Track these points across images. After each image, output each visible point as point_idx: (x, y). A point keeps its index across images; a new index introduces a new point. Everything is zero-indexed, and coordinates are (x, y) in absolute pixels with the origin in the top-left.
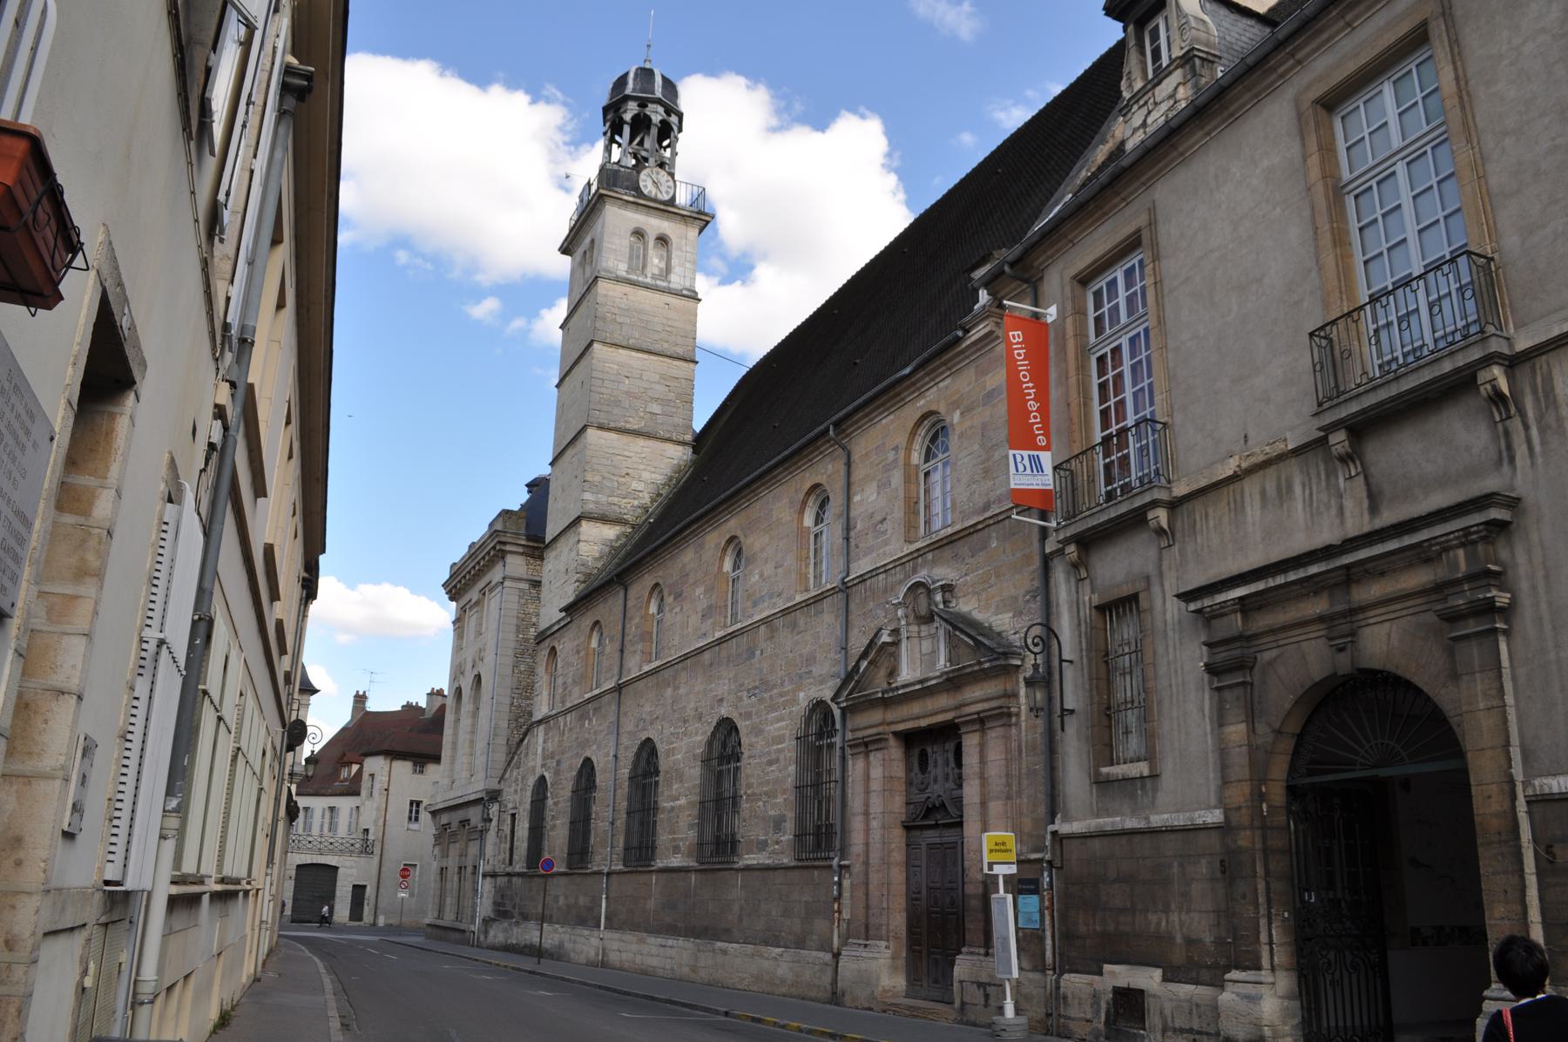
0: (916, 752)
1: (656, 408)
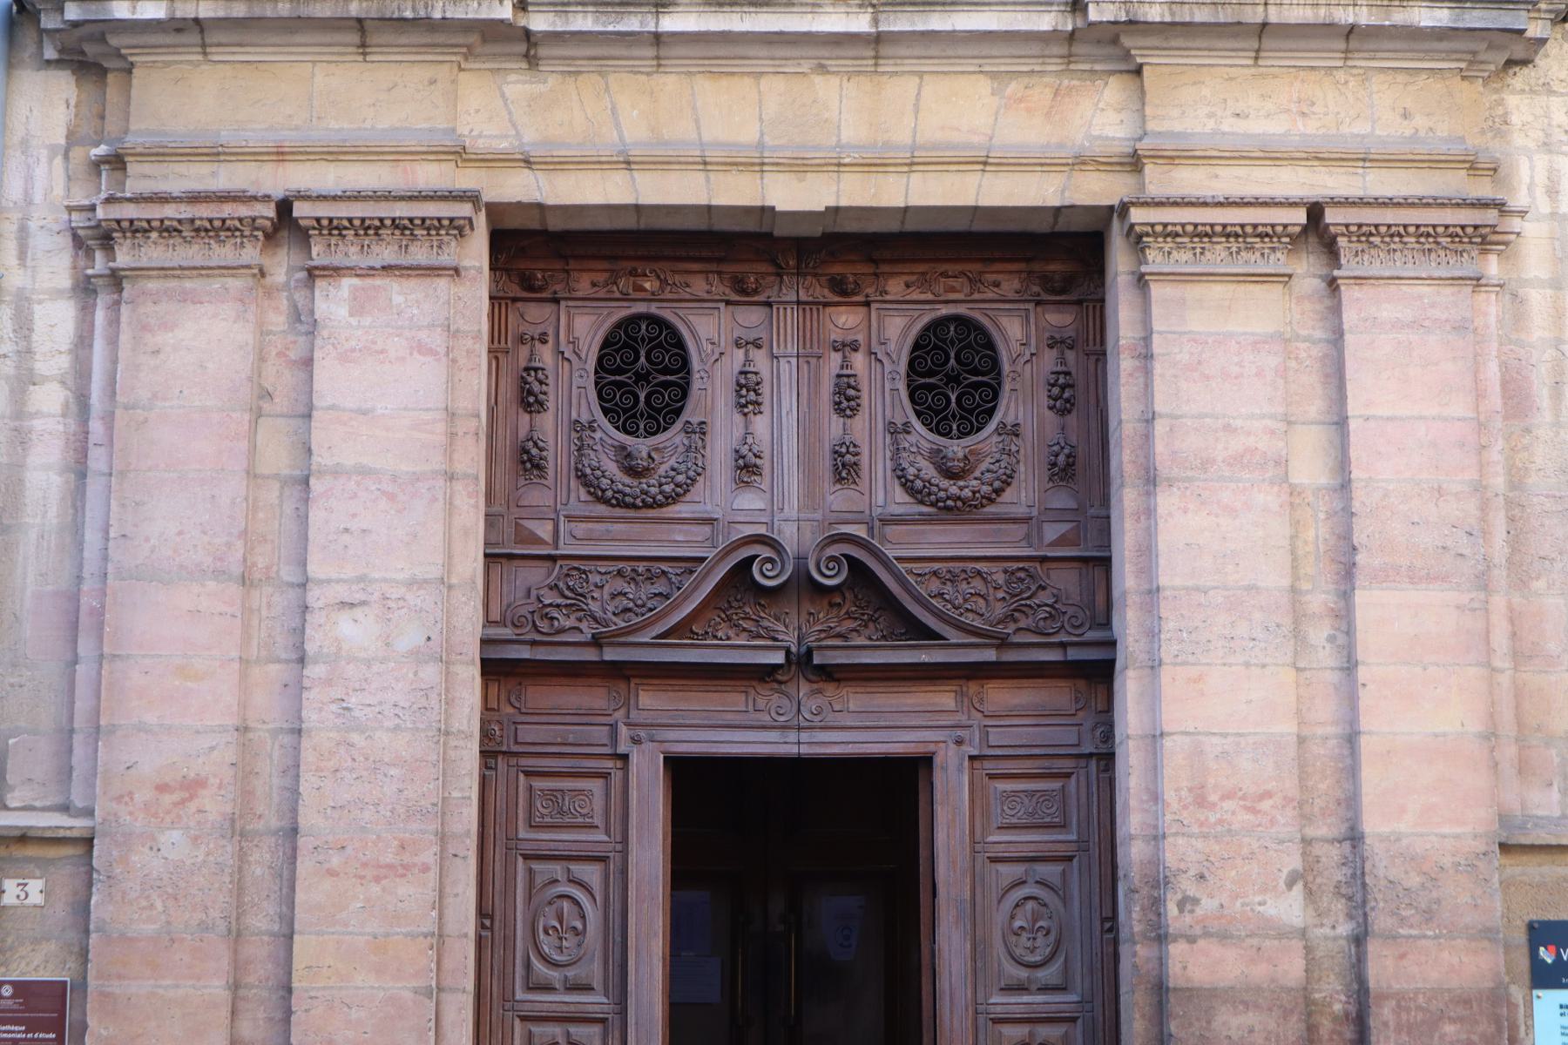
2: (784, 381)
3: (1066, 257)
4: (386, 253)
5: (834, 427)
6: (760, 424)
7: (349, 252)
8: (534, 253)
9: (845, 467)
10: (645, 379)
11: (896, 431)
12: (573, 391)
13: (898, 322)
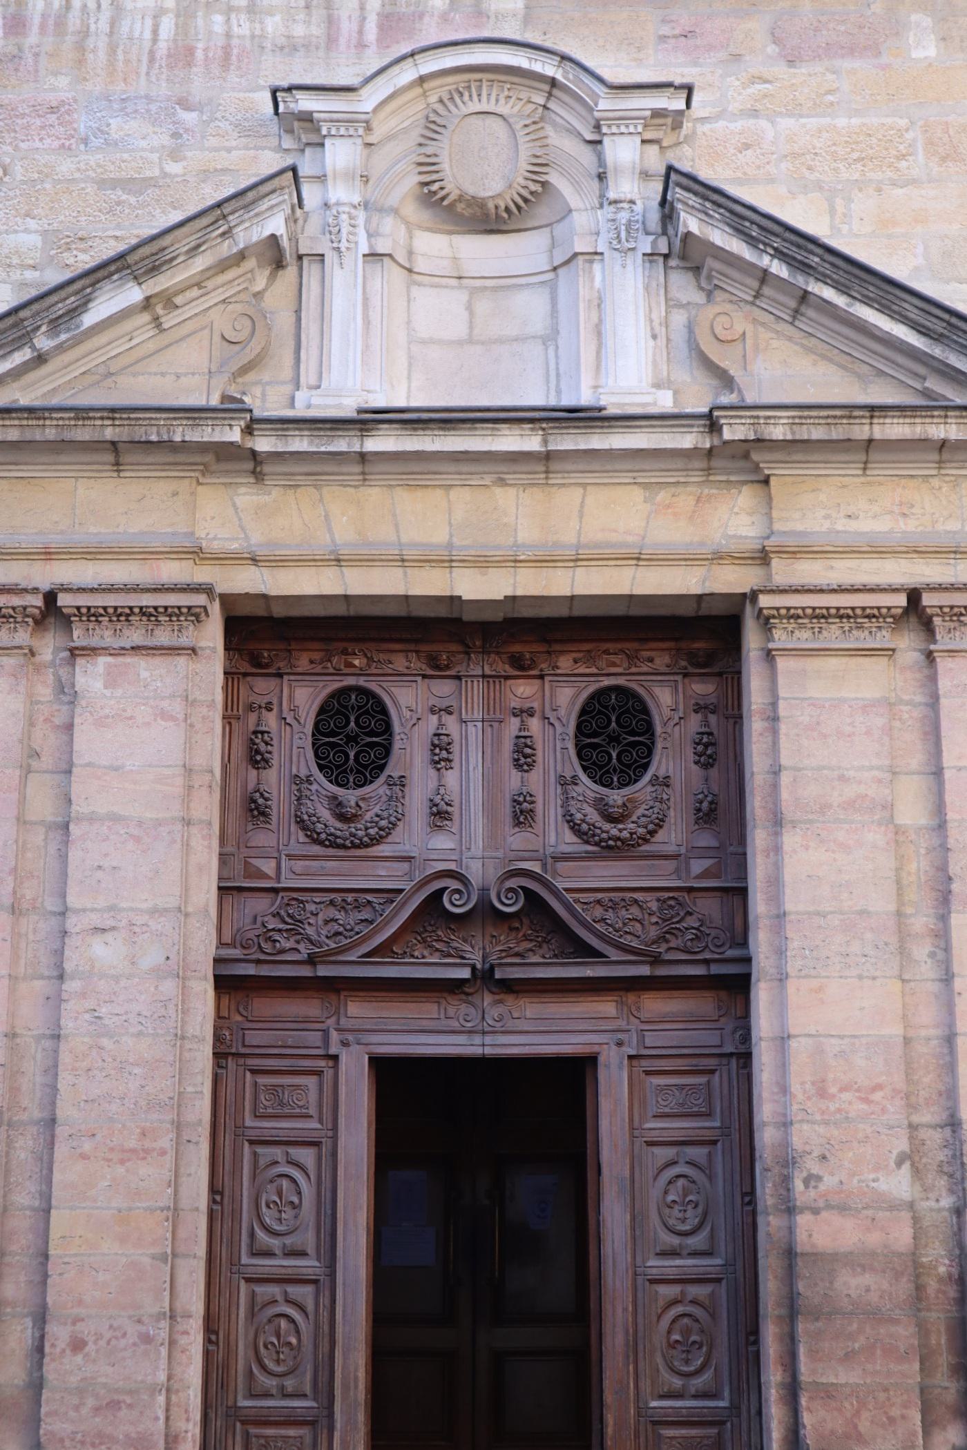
0: (305, 698)
2: (471, 742)
3: (708, 636)
4: (135, 635)
5: (514, 780)
6: (451, 778)
7: (105, 636)
8: (262, 636)
9: (524, 813)
10: (354, 741)
11: (565, 783)
12: (294, 750)
13: (565, 694)
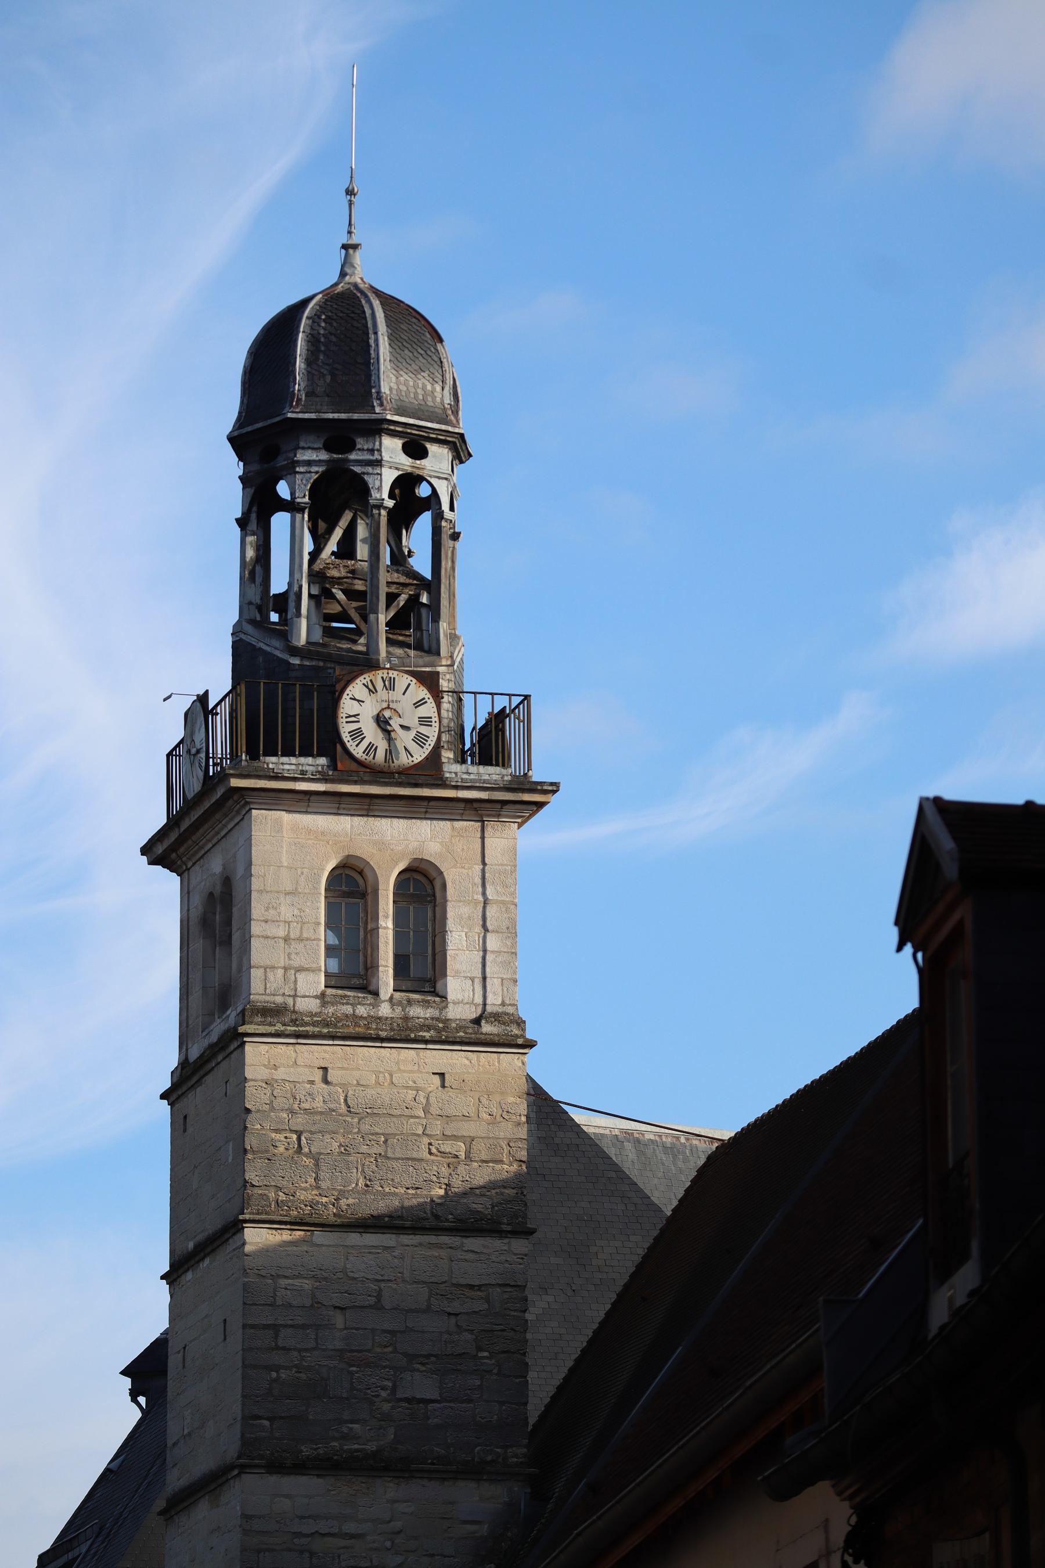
1: (422, 1385)
